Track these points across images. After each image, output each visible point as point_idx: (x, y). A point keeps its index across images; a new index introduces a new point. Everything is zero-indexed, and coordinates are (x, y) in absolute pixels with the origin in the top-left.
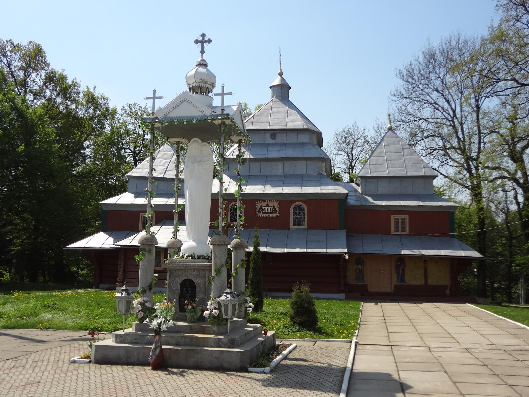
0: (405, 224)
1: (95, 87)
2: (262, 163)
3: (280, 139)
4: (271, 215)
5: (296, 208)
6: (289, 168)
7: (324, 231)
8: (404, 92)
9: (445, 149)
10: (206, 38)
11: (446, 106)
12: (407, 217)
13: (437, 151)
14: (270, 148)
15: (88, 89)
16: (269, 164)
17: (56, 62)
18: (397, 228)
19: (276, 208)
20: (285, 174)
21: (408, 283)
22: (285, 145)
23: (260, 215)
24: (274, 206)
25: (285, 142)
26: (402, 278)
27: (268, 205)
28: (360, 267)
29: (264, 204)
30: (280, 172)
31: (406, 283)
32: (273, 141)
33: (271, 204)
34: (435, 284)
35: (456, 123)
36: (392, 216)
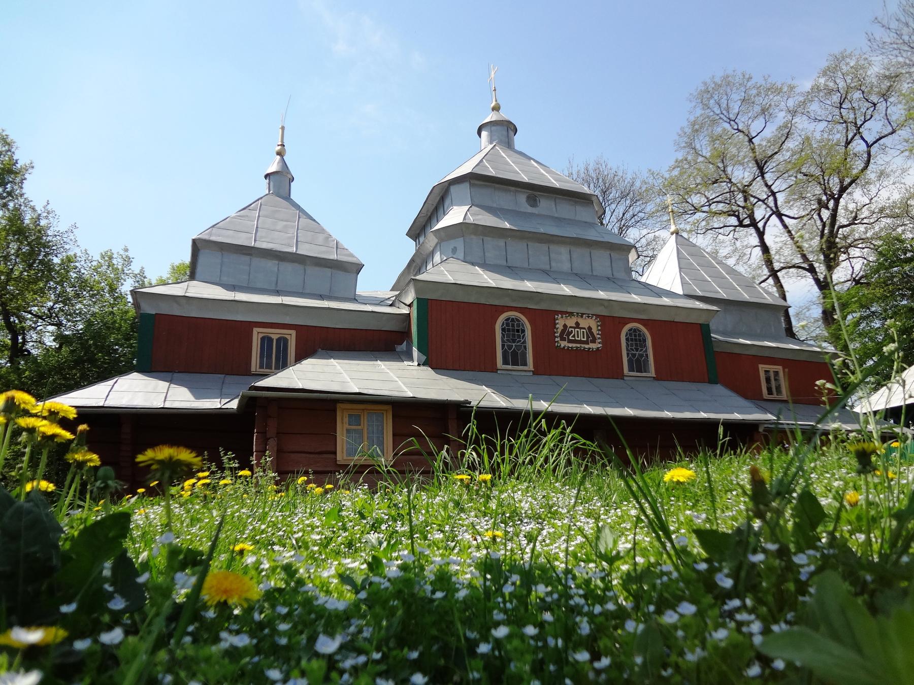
4: (587, 346)
5: (631, 335)
10: (766, 77)
12: (293, 332)
13: (820, 227)
19: (594, 330)
23: (563, 344)
24: (590, 328)
27: (577, 324)
29: (571, 322)
33: (584, 323)
36: (761, 366)
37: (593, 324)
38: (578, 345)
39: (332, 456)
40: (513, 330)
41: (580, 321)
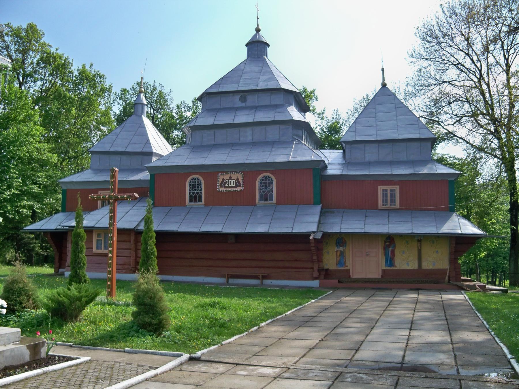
0: (395, 196)
1: (92, 65)
2: (228, 129)
3: (251, 100)
5: (263, 180)
6: (259, 134)
7: (295, 207)
8: (423, 52)
9: (474, 115)
11: (472, 67)
12: (397, 188)
14: (238, 113)
15: (84, 66)
16: (237, 130)
17: (55, 42)
18: (385, 202)
19: (241, 181)
20: (254, 141)
21: (398, 268)
22: (256, 108)
23: (223, 189)
24: (238, 179)
25: (257, 105)
26: (390, 261)
27: (230, 178)
28: (341, 249)
30: (249, 139)
31: (396, 267)
32: (243, 105)
33: (234, 176)
34: (431, 267)
35: (484, 87)
36: (379, 187)
37: (240, 177)
38: (230, 189)
39: (119, 255)
40: (195, 185)
41: (232, 175)
